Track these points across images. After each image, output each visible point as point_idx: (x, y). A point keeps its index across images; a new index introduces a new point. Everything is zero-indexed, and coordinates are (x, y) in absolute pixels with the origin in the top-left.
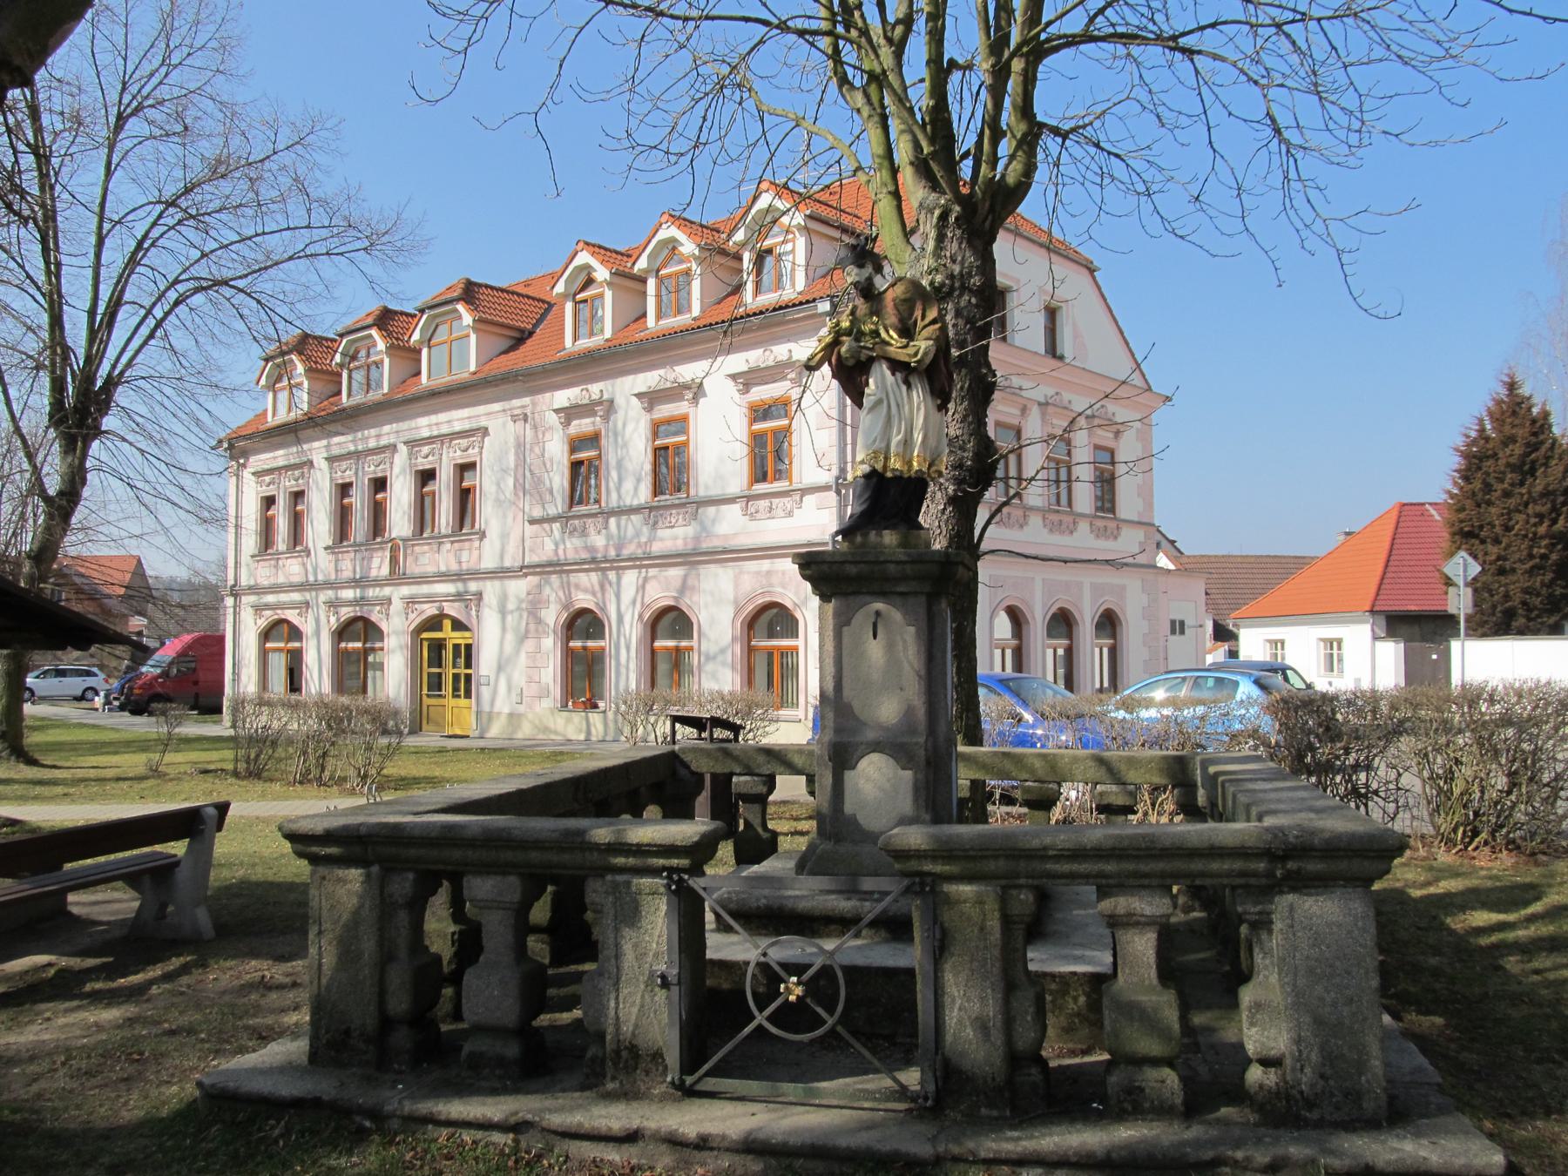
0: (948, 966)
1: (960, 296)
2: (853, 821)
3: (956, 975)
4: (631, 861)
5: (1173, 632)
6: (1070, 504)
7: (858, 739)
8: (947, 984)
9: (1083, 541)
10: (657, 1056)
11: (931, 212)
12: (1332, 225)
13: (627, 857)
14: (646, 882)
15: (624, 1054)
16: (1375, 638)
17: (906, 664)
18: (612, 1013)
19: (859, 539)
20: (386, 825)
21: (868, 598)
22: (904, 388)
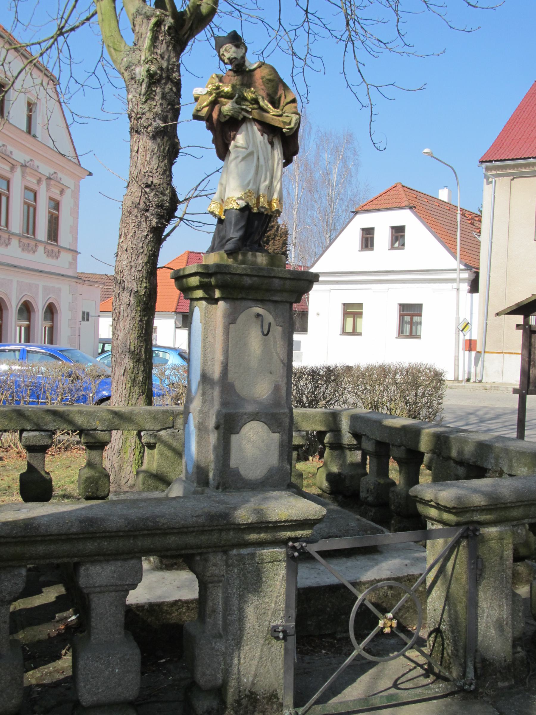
0: (481, 588)
1: (166, 84)
2: (236, 473)
3: (485, 593)
4: (263, 536)
5: (83, 319)
6: (34, 234)
7: (242, 411)
8: (480, 600)
9: (39, 258)
10: (272, 697)
11: (148, 18)
12: (372, 90)
13: (259, 533)
14: (267, 552)
15: (244, 702)
16: (177, 327)
17: (275, 355)
18: (235, 670)
19: (240, 257)
20: (14, 524)
21: (249, 303)
22: (269, 146)
